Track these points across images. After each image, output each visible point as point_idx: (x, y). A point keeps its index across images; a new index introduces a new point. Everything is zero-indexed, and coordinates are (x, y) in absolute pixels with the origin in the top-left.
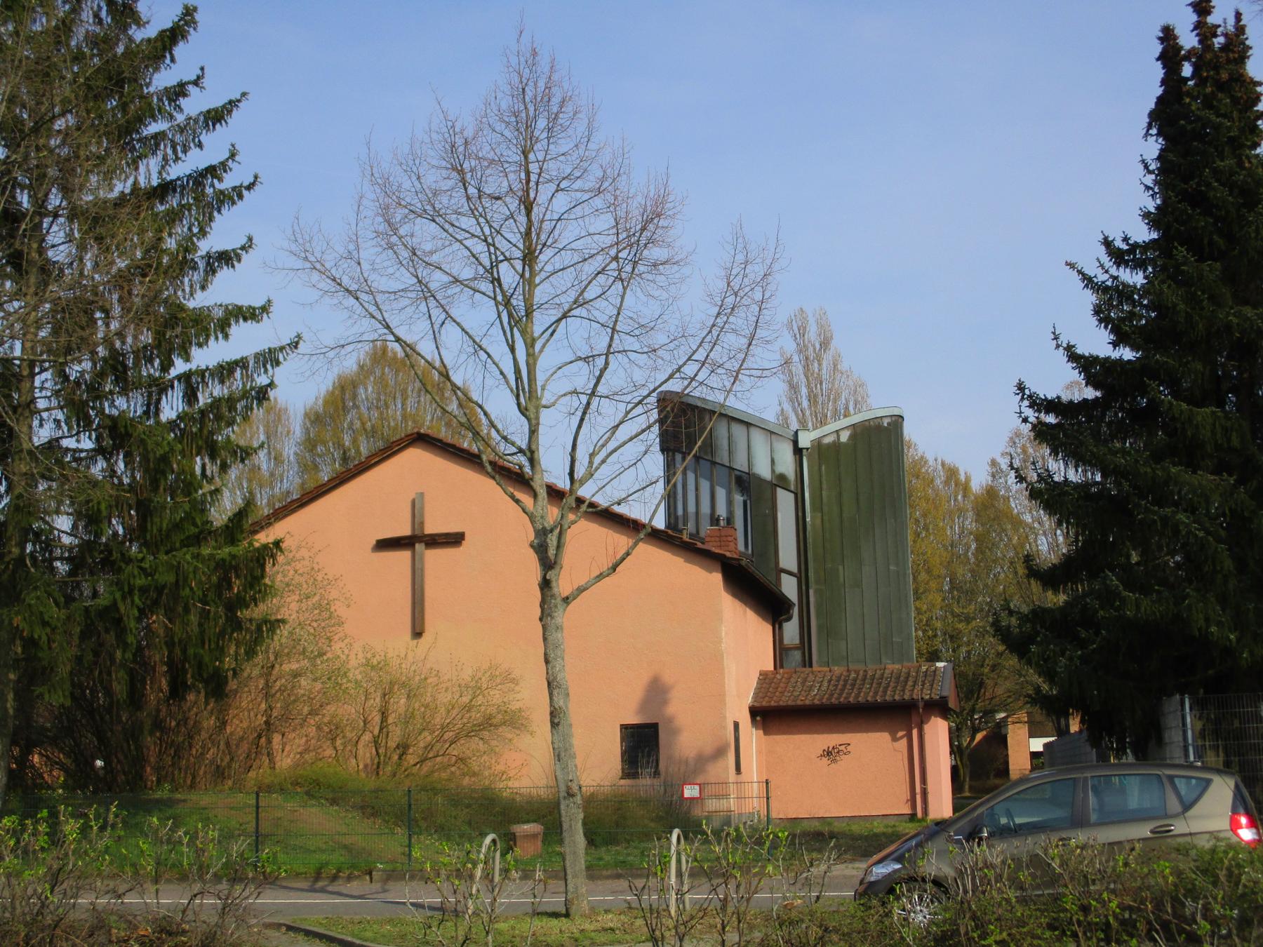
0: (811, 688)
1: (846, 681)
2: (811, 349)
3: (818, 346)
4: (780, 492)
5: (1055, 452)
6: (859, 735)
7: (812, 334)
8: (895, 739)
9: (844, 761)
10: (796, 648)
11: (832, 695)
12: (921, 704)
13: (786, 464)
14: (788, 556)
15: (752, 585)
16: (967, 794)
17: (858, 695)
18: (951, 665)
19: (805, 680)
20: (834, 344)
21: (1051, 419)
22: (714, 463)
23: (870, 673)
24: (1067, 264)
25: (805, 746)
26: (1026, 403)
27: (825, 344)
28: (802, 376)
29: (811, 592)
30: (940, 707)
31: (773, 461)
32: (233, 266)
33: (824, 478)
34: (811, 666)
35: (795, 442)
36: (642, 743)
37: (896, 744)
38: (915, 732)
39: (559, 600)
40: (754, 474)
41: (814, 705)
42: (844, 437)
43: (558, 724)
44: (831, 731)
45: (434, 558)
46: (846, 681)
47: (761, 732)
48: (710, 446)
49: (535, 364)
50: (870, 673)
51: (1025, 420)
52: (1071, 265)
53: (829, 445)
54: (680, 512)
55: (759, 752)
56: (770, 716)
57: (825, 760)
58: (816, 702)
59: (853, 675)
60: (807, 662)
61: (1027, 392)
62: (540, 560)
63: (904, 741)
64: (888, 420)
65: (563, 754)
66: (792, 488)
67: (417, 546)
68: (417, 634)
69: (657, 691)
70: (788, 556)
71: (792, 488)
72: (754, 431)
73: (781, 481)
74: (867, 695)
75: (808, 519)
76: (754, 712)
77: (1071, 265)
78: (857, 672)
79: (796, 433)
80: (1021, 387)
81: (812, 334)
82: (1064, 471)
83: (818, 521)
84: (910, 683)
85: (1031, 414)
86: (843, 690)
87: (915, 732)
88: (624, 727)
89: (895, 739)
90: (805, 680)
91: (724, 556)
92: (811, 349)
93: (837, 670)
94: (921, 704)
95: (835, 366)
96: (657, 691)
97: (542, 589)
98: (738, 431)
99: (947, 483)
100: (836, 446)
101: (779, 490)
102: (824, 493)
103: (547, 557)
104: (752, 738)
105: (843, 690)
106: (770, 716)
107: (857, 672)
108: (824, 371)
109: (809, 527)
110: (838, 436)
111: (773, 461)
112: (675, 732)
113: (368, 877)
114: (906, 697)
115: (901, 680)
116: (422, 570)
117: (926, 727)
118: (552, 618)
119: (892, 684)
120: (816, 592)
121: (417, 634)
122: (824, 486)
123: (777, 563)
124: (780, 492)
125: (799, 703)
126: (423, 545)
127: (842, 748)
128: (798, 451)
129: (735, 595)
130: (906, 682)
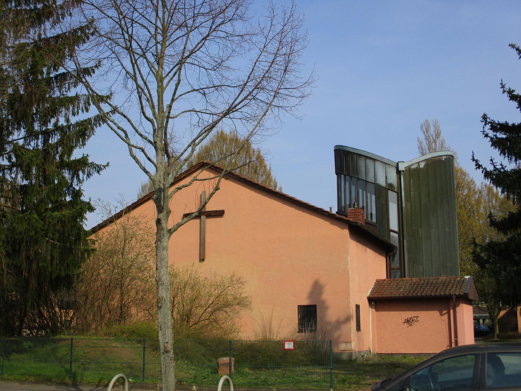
0: (400, 288)
1: (418, 285)
2: (431, 137)
3: (434, 136)
4: (390, 192)
5: (503, 152)
6: (423, 312)
7: (432, 130)
8: (442, 315)
9: (415, 325)
10: (397, 269)
11: (409, 292)
12: (454, 297)
13: (393, 179)
14: (394, 224)
15: (368, 235)
16: (496, 339)
17: (422, 292)
18: (472, 277)
19: (398, 284)
20: (442, 135)
21: (501, 135)
22: (358, 179)
23: (431, 281)
24: (510, 45)
25: (396, 317)
26: (488, 126)
27: (438, 135)
28: (427, 150)
29: (405, 241)
30: (465, 299)
31: (386, 177)
32: (91, 75)
33: (412, 185)
34: (405, 277)
35: (397, 168)
36: (308, 314)
37: (443, 317)
38: (452, 311)
39: (165, 232)
40: (377, 184)
41: (400, 297)
42: (422, 165)
43: (161, 307)
44: (415, 311)
45: (210, 223)
46: (418, 285)
47: (374, 310)
48: (357, 171)
49: (162, 94)
50: (431, 281)
51: (486, 136)
52: (512, 46)
53: (414, 169)
54: (343, 205)
55: (373, 320)
56: (378, 301)
57: (406, 325)
58: (401, 295)
59: (422, 282)
60: (403, 275)
61: (488, 120)
62: (157, 207)
63: (446, 316)
64: (445, 157)
65: (163, 326)
66: (396, 190)
67: (202, 217)
68: (202, 260)
69: (317, 288)
70: (394, 224)
71: (396, 190)
72: (378, 164)
73: (390, 187)
74: (428, 292)
75: (404, 206)
76: (371, 300)
77: (512, 46)
78: (424, 280)
79: (398, 164)
80: (485, 117)
81: (432, 130)
82: (510, 165)
83: (409, 206)
84: (450, 286)
85: (491, 134)
86: (415, 289)
87: (452, 311)
88: (300, 307)
89: (442, 315)
90: (398, 284)
91: (349, 221)
92: (431, 137)
93: (414, 279)
94: (454, 297)
95: (442, 145)
96: (317, 288)
97: (157, 225)
98: (370, 163)
99: (488, 195)
100: (418, 169)
101: (389, 191)
102: (411, 192)
103: (161, 205)
104: (368, 314)
105: (415, 289)
106: (378, 301)
107: (424, 280)
108: (437, 148)
109: (404, 209)
110: (419, 165)
111: (386, 177)
112: (326, 308)
113: (122, 386)
114: (447, 293)
115: (446, 285)
116: (204, 228)
117: (458, 309)
118: (161, 242)
119: (441, 287)
120: (407, 241)
121: (202, 260)
122: (412, 189)
123: (388, 226)
124: (390, 192)
125: (393, 295)
126: (205, 217)
127: (414, 319)
128: (399, 172)
129: (358, 241)
130: (448, 286)
